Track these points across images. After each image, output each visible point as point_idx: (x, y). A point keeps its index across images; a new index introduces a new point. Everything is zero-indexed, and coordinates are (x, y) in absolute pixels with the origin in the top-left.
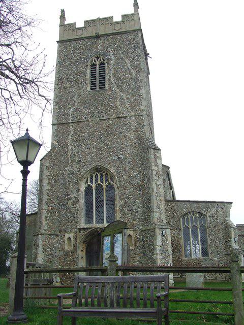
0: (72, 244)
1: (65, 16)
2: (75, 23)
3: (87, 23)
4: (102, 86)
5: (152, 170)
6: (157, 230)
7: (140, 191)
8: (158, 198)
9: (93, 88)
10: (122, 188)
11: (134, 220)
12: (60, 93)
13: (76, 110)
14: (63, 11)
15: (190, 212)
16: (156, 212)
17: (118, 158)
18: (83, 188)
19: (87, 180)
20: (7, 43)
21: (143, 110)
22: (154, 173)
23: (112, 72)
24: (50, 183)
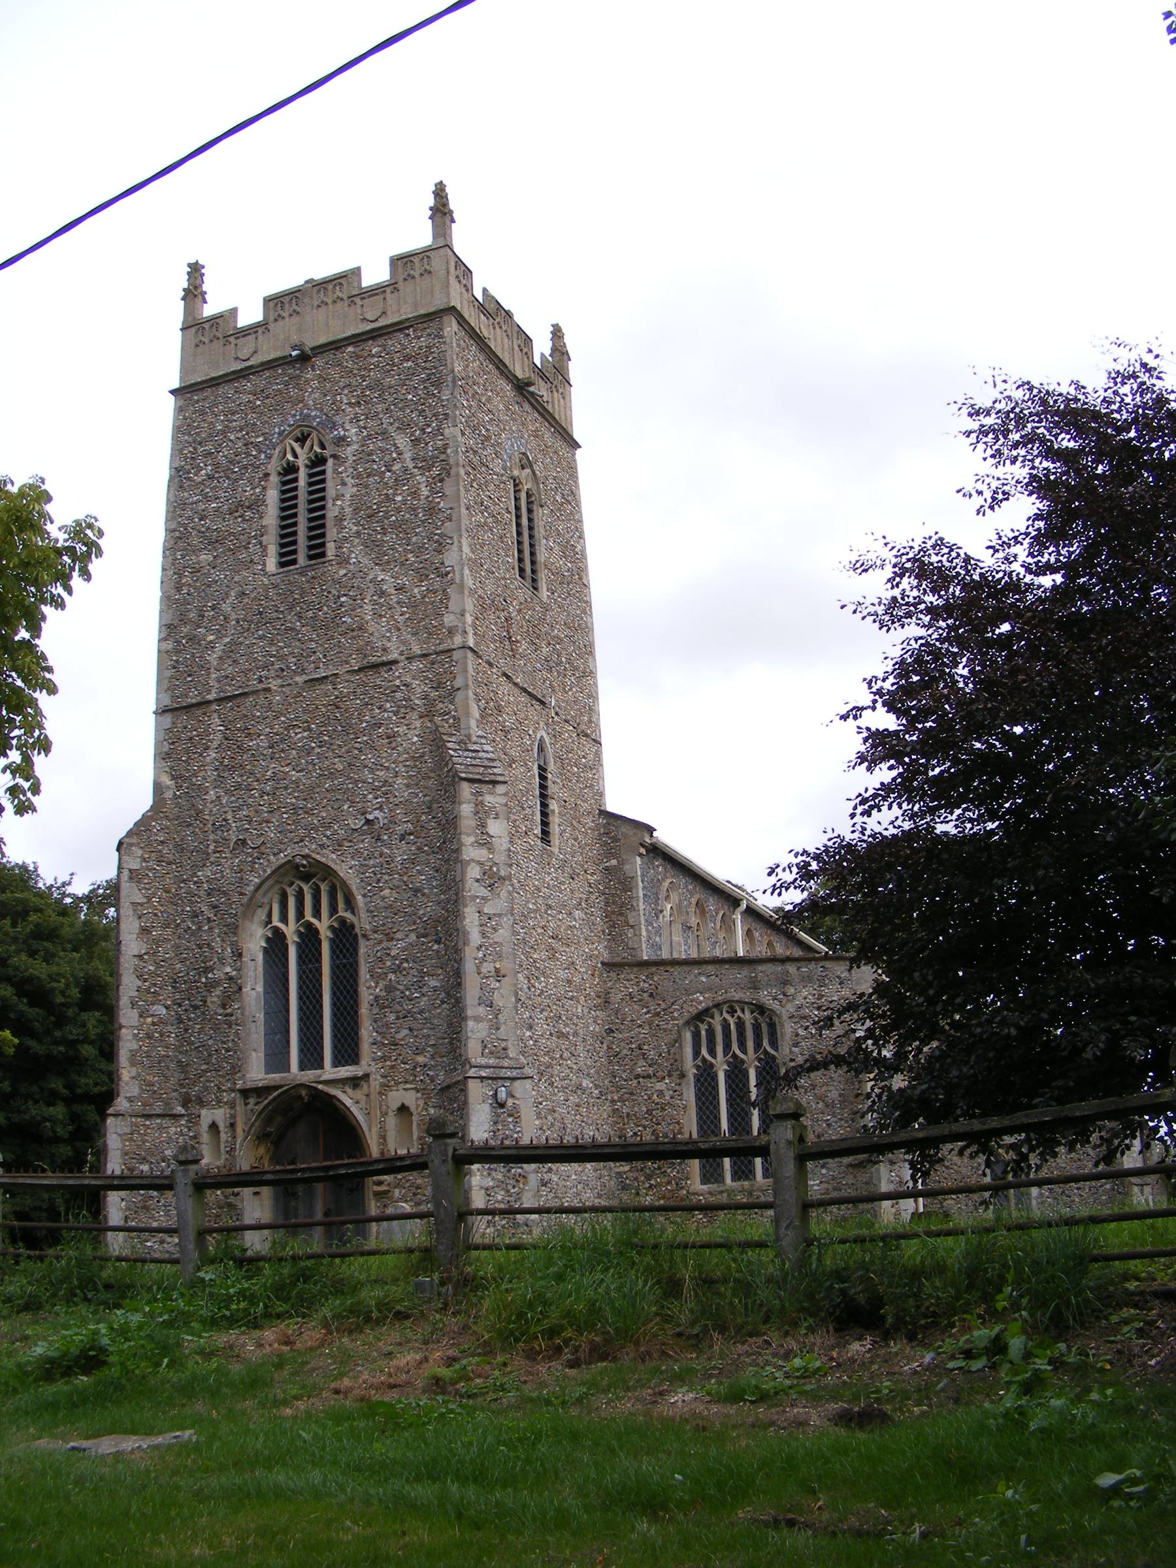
0: (222, 1146)
1: (452, 206)
2: (234, 312)
3: (276, 303)
4: (317, 552)
5: (465, 864)
6: (474, 1088)
7: (438, 942)
8: (487, 968)
9: (287, 559)
10: (378, 936)
11: (419, 1051)
12: (179, 589)
13: (231, 650)
14: (196, 271)
15: (717, 1006)
16: (477, 1019)
17: (368, 822)
18: (255, 941)
19: (270, 915)
20: (251, 350)
21: (451, 632)
22: (474, 872)
23: (350, 491)
24: (145, 931)
